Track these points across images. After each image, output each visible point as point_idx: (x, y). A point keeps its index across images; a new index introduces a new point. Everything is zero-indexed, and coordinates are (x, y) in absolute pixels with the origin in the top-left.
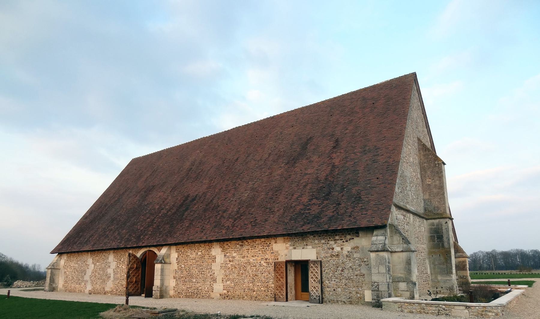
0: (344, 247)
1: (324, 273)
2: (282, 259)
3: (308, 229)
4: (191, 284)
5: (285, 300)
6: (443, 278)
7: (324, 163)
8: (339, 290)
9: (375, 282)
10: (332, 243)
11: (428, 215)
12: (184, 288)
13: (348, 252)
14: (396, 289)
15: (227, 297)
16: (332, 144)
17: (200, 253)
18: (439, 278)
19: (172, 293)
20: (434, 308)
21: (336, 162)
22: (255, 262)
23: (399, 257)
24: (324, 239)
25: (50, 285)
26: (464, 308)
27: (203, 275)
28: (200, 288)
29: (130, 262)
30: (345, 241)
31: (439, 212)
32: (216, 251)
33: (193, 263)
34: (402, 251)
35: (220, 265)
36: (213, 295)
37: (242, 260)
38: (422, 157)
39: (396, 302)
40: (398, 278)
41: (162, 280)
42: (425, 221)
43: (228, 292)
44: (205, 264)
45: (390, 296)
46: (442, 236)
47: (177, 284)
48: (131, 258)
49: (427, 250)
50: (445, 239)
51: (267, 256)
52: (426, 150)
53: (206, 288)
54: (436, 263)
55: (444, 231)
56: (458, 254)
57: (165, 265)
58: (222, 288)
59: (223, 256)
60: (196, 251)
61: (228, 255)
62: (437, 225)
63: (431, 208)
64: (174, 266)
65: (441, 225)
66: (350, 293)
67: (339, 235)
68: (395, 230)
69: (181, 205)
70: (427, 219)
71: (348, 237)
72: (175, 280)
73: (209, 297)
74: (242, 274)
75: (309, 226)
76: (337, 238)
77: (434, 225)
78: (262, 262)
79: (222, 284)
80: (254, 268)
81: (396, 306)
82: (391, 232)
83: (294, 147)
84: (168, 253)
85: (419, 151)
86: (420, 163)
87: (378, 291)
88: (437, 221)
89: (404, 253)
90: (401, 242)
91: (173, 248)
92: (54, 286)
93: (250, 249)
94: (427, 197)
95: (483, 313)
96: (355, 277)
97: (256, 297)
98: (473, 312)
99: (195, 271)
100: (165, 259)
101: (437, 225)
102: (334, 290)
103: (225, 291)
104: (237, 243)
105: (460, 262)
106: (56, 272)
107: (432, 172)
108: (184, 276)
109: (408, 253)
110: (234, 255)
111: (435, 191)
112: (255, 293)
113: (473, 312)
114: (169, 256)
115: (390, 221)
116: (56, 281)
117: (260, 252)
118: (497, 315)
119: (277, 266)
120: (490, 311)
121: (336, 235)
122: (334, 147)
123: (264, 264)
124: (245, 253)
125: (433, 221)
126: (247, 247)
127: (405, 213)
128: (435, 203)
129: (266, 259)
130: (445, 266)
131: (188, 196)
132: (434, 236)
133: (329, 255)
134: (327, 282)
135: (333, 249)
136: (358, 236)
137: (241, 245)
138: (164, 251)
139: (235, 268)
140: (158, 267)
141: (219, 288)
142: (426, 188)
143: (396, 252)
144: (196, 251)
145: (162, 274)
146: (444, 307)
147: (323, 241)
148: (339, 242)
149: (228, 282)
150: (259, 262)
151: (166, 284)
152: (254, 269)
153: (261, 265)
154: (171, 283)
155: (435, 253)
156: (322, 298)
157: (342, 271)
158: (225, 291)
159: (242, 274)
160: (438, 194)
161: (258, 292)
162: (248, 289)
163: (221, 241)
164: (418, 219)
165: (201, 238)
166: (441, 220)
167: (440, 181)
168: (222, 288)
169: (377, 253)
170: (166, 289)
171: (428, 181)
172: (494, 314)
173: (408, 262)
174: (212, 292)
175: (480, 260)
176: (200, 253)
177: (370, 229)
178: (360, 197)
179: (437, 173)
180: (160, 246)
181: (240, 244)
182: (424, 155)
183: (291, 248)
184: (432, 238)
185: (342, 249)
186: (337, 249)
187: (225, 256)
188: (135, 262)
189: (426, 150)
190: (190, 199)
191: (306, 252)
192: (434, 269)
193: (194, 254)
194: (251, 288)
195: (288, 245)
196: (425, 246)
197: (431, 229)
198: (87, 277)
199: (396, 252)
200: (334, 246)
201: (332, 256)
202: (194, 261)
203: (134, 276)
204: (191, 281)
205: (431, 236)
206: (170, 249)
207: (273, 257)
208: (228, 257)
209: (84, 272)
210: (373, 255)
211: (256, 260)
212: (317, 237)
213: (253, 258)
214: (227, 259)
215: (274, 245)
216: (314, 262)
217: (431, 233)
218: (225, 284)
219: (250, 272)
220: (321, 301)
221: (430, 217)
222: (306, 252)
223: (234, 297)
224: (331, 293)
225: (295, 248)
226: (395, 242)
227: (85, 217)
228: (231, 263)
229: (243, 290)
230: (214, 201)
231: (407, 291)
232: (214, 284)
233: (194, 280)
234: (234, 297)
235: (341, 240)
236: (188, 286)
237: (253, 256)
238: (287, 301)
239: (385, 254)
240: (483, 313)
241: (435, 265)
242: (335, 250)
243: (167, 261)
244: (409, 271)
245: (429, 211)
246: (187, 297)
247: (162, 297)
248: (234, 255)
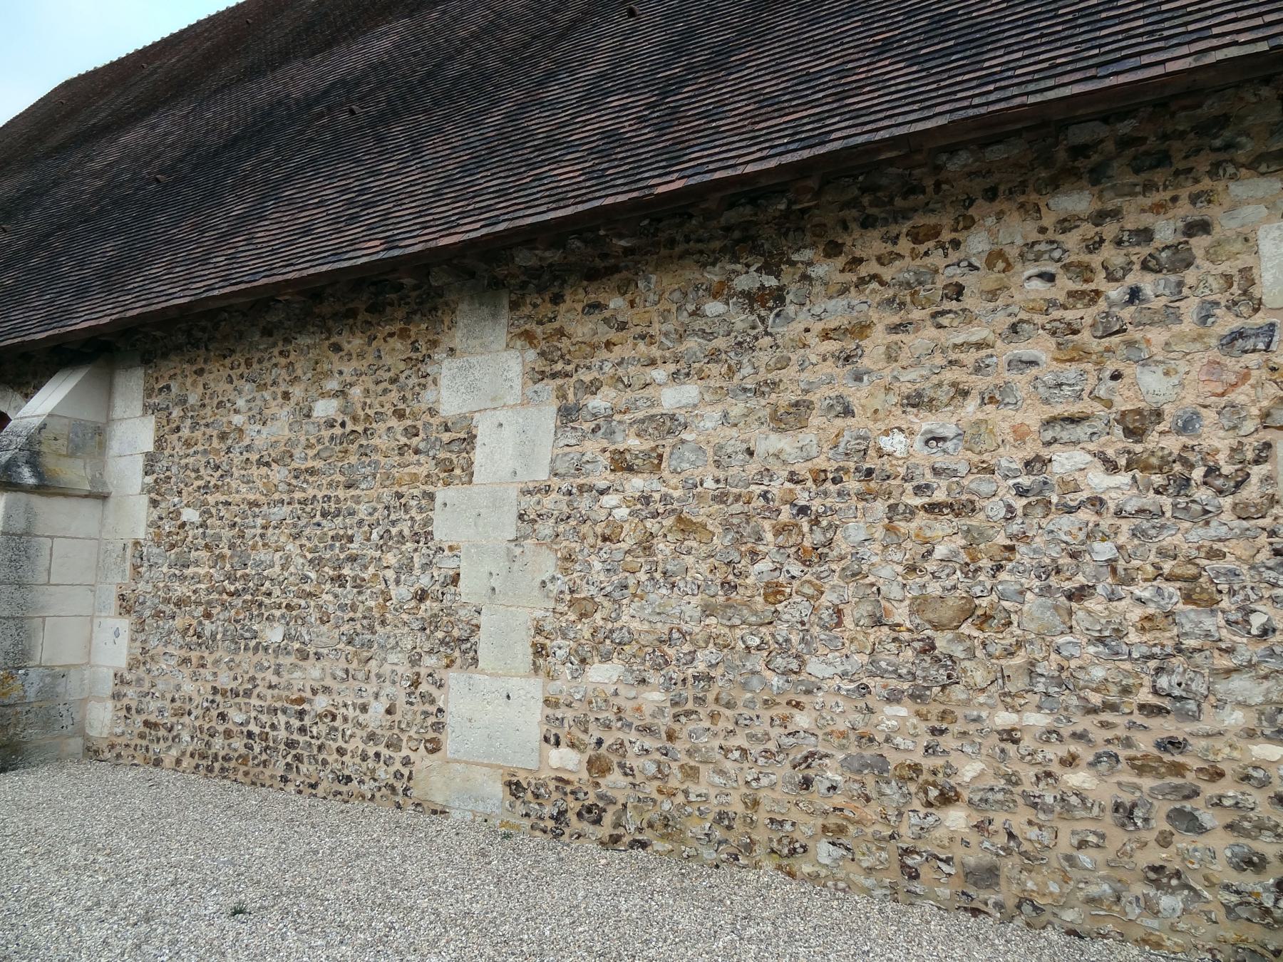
4: (246, 660)
12: (189, 688)
15: (592, 814)
17: (325, 408)
19: (102, 719)
22: (958, 458)
27: (348, 594)
32: (484, 381)
33: (272, 488)
36: (433, 779)
43: (597, 766)
44: (369, 499)
47: (141, 659)
51: (1151, 385)
53: (378, 708)
57: (51, 512)
58: (532, 720)
59: (548, 414)
60: (297, 391)
61: (598, 403)
64: (133, 516)
69: (317, 101)
72: (125, 624)
73: (399, 791)
74: (774, 592)
78: (1065, 461)
79: (532, 690)
80: (941, 527)
84: (88, 414)
91: (131, 389)
93: (882, 319)
97: (988, 875)
99: (283, 558)
100: (49, 462)
103: (565, 760)
104: (713, 276)
108: (198, 598)
110: (674, 397)
112: (957, 819)
114: (92, 439)
117: (1040, 347)
123: (1098, 480)
126: (837, 312)
137: (753, 299)
139: (686, 526)
141: (498, 717)
144: (297, 391)
149: (603, 674)
150: (1011, 458)
152: (946, 538)
153: (1038, 494)
158: (565, 760)
159: (774, 592)
161: (1019, 819)
162: (856, 767)
163: (543, 270)
168: (530, 719)
170: (48, 693)
174: (434, 747)
176: (325, 408)
181: (746, 282)
187: (568, 414)
193: (277, 415)
194: (910, 749)
202: (278, 474)
208: (603, 425)
211: (970, 436)
213: (925, 422)
214: (592, 447)
218: (563, 685)
219: (887, 572)
228: (637, 483)
229: (783, 771)
232: (454, 678)
233: (274, 635)
236: (225, 681)
237: (916, 401)
243: (74, 473)
246: (210, 764)
248: (674, 397)
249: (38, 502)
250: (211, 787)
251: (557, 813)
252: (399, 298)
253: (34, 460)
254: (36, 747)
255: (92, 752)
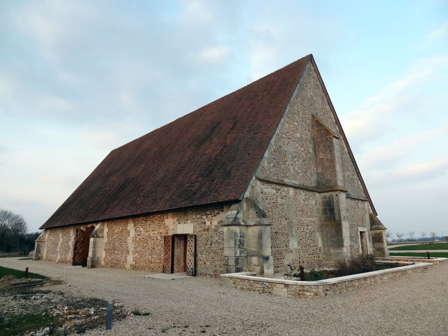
0: (213, 221)
1: (198, 246)
2: (171, 233)
3: (184, 205)
4: (114, 255)
5: (170, 272)
6: (334, 251)
7: (220, 143)
8: (208, 263)
9: (226, 256)
10: (204, 217)
11: (322, 189)
13: (216, 226)
14: (249, 263)
15: (135, 267)
16: (231, 126)
17: (121, 228)
18: (332, 251)
19: (103, 263)
20: (260, 286)
21: (228, 142)
23: (253, 231)
24: (199, 214)
25: (36, 254)
26: (282, 286)
28: (119, 259)
29: (77, 236)
30: (213, 215)
31: (330, 185)
32: (131, 226)
34: (255, 225)
35: (132, 239)
36: (126, 267)
37: (146, 234)
38: (316, 133)
39: (231, 278)
40: (252, 252)
41: (94, 252)
42: (317, 194)
43: (136, 263)
45: (238, 270)
46: (333, 208)
48: (79, 233)
49: (317, 222)
50: (336, 211)
52: (319, 126)
54: (329, 236)
55: (335, 203)
56: (374, 226)
57: (98, 239)
62: (329, 198)
63: (324, 181)
65: (333, 198)
66: (216, 266)
67: (209, 210)
68: (253, 203)
70: (320, 193)
71: (216, 211)
72: (105, 252)
75: (186, 202)
76: (208, 212)
77: (326, 198)
78: (158, 236)
81: (232, 281)
82: (248, 205)
83: (206, 131)
84: (102, 228)
85: (313, 127)
86: (313, 139)
87: (228, 265)
88: (328, 194)
89: (257, 227)
90: (255, 216)
91: (106, 224)
92: (40, 255)
94: (320, 171)
95: (301, 293)
96: (220, 251)
97: (153, 269)
98: (291, 291)
100: (98, 234)
101: (329, 198)
102: (204, 263)
103: (134, 262)
105: (376, 234)
106: (42, 244)
107: (324, 146)
109: (260, 226)
111: (327, 164)
113: (291, 291)
114: (102, 231)
115: (247, 194)
116: (42, 252)
118: (317, 295)
119: (166, 238)
120: (308, 291)
121: (207, 210)
122: (232, 129)
124: (148, 228)
125: (326, 194)
127: (278, 187)
128: (328, 176)
129: (161, 233)
130: (336, 239)
131: (128, 179)
132: (326, 209)
133: (202, 229)
134: (200, 255)
135: (205, 223)
136: (223, 211)
138: (97, 227)
139: (141, 241)
140: (92, 240)
142: (319, 162)
143: (250, 226)
145: (94, 247)
146: (267, 284)
147: (198, 216)
148: (209, 216)
149: (136, 254)
151: (98, 255)
154: (102, 255)
155: (327, 225)
156: (196, 271)
157: (211, 245)
159: (145, 247)
160: (330, 167)
163: (134, 217)
164: (302, 194)
165: (118, 215)
166: (333, 193)
167: (331, 154)
169: (229, 227)
170: (98, 260)
171: (321, 155)
172: (312, 294)
173: (260, 237)
175: (25, 236)
177: (229, 203)
178: (230, 173)
179: (329, 147)
180: (97, 222)
182: (318, 131)
183: (177, 223)
184: (325, 210)
185: (211, 223)
186: (208, 223)
187: (136, 230)
188: (82, 236)
189: (319, 126)
190: (128, 181)
191: (186, 227)
192: (327, 241)
193: (117, 228)
195: (175, 220)
196: (315, 219)
197: (324, 202)
198: (58, 249)
199: (250, 226)
200: (206, 220)
201: (204, 230)
202: (117, 235)
203: (81, 248)
204: (114, 253)
205: (324, 209)
206: (103, 224)
207: (165, 232)
209: (57, 244)
210: (225, 229)
211: (154, 233)
212: (194, 212)
213: (153, 233)
215: (166, 220)
216: (191, 236)
217: (324, 206)
220: (195, 274)
221: (322, 191)
222: (186, 227)
223: (139, 268)
224: (202, 266)
225: (179, 223)
226: (251, 216)
227: (69, 199)
230: (140, 183)
231: (258, 265)
234: (139, 268)
235: (211, 214)
238: (172, 272)
239: (237, 229)
240: (301, 293)
241: (327, 238)
242: (207, 225)
243: (100, 235)
244: (260, 245)
245: (322, 184)
246: (112, 267)
247: (93, 266)
248: (141, 229)
249: (97, 238)
250: (113, 269)
251: (134, 267)
252: (126, 218)
253: (96, 234)
254: (352, 258)
255: (102, 267)
